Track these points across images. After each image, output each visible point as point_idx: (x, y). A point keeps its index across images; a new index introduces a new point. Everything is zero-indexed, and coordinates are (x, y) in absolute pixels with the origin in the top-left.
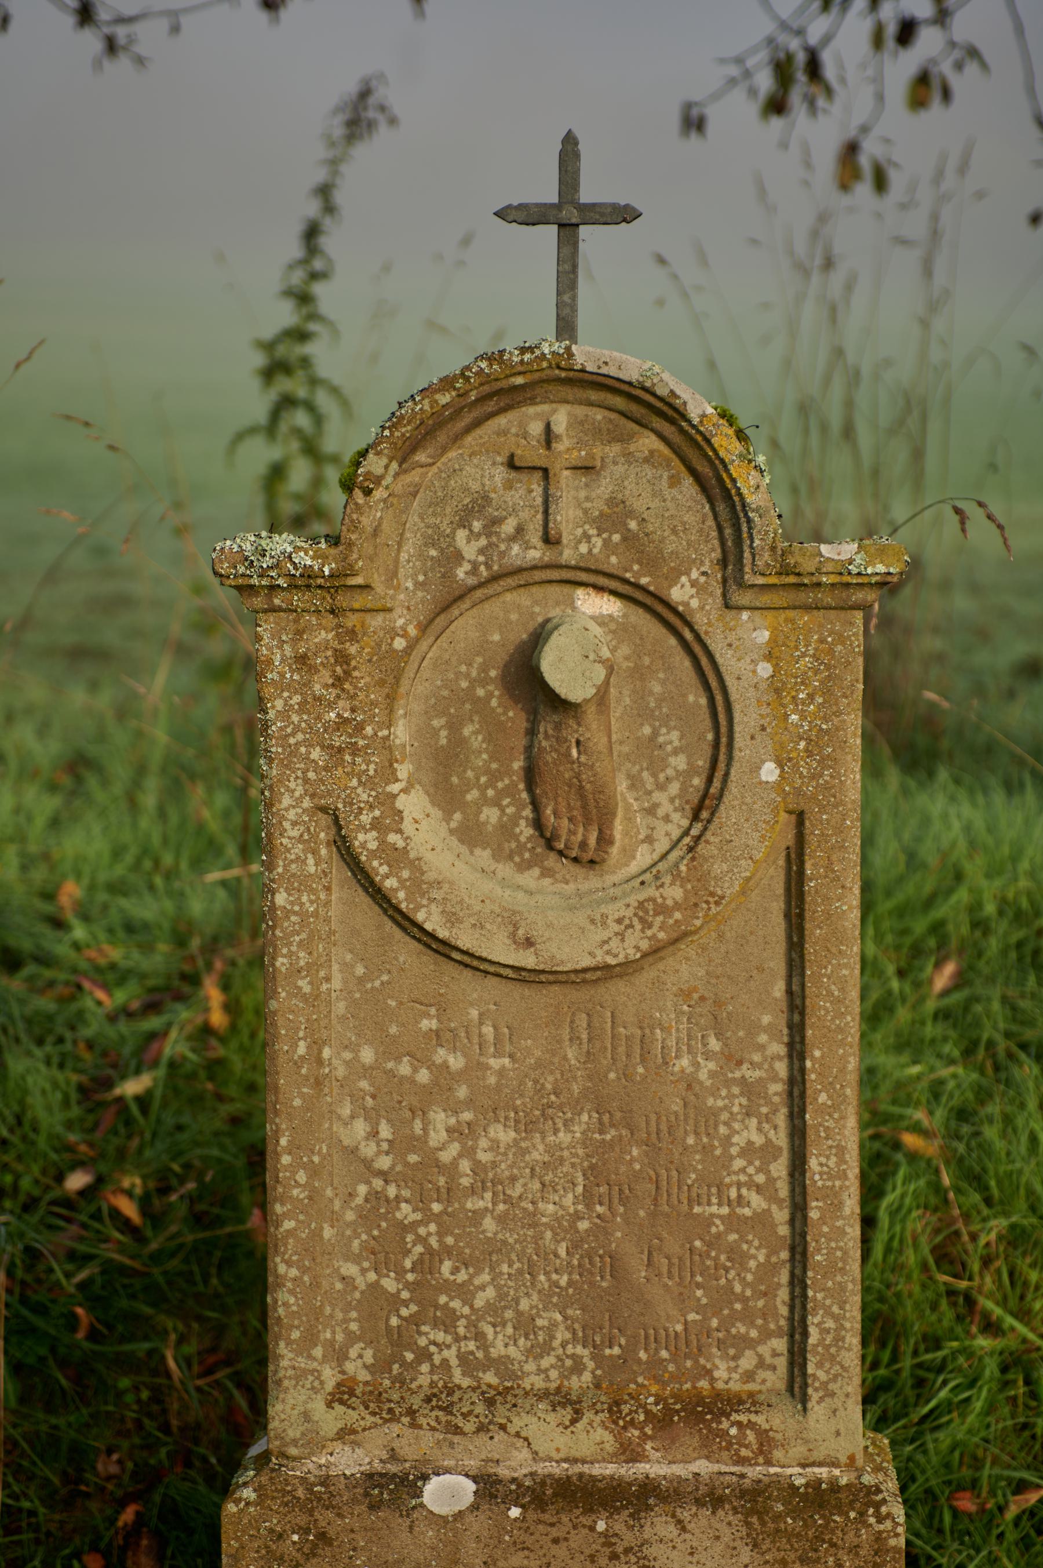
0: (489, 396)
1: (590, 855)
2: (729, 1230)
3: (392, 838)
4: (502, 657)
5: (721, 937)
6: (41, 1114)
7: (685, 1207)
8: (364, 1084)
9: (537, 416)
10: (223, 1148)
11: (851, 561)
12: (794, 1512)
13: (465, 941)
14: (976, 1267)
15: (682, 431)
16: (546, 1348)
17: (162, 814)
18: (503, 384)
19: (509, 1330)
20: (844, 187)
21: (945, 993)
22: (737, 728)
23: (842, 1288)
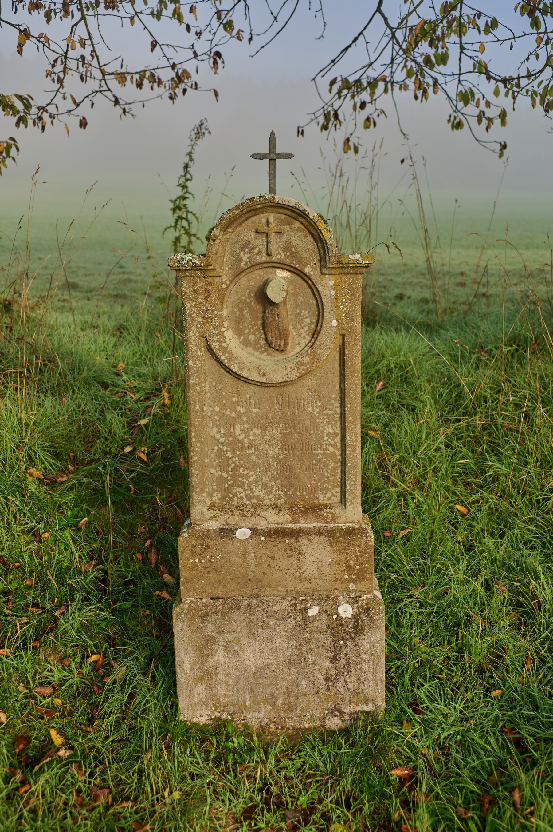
0: (250, 211)
1: (282, 348)
2: (323, 457)
3: (223, 344)
4: (255, 290)
5: (320, 372)
6: (117, 430)
7: (310, 451)
8: (216, 417)
9: (264, 217)
10: (171, 439)
11: (358, 260)
12: (342, 536)
13: (245, 374)
14: (390, 468)
15: (308, 221)
16: (271, 492)
17: (147, 342)
18: (254, 207)
19: (260, 487)
20: (345, 152)
21: (380, 390)
22: (325, 310)
23: (356, 473)
